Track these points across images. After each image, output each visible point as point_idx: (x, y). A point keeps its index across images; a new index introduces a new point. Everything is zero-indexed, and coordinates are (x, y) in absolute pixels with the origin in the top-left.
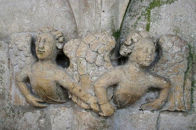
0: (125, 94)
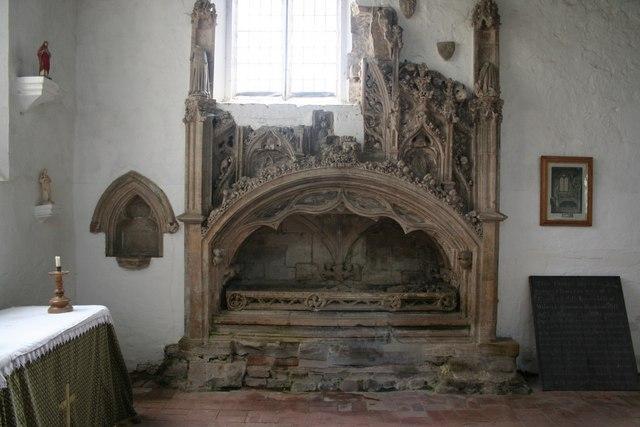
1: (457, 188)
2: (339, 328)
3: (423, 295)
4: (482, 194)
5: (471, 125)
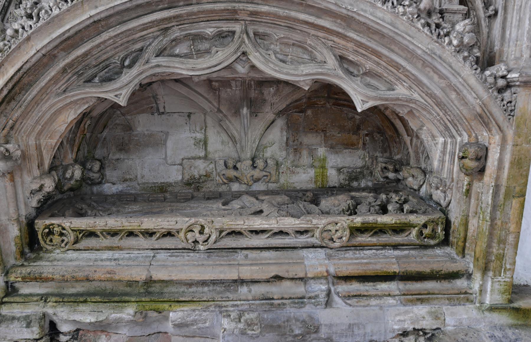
0: (493, 65)
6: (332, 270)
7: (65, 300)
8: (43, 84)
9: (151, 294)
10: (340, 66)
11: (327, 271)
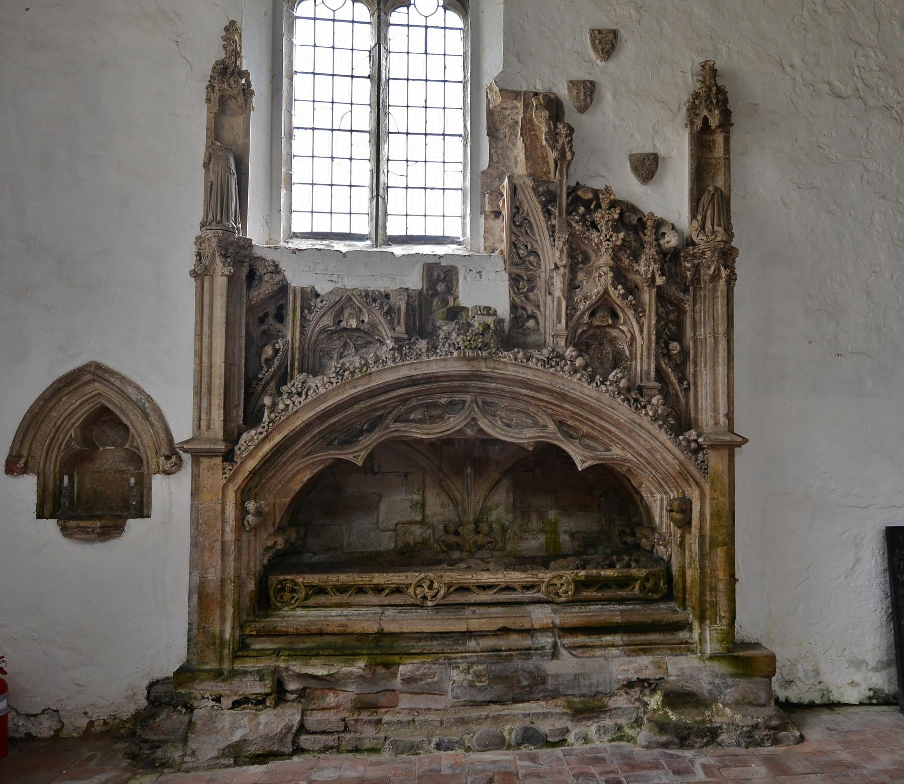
1: (665, 392)
2: (469, 634)
3: (609, 573)
4: (705, 402)
5: (686, 291)
6: (557, 622)
7: (298, 653)
8: (297, 448)
9: (383, 649)
10: (559, 430)
11: (553, 623)
